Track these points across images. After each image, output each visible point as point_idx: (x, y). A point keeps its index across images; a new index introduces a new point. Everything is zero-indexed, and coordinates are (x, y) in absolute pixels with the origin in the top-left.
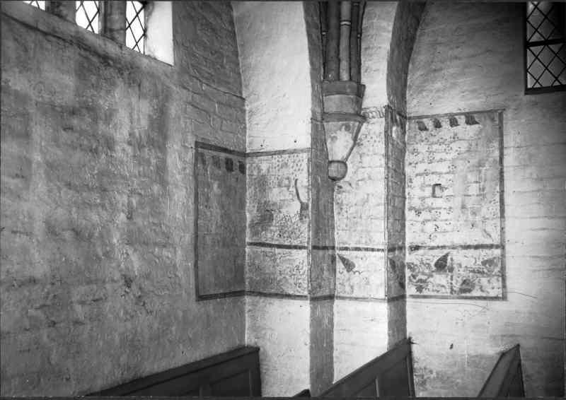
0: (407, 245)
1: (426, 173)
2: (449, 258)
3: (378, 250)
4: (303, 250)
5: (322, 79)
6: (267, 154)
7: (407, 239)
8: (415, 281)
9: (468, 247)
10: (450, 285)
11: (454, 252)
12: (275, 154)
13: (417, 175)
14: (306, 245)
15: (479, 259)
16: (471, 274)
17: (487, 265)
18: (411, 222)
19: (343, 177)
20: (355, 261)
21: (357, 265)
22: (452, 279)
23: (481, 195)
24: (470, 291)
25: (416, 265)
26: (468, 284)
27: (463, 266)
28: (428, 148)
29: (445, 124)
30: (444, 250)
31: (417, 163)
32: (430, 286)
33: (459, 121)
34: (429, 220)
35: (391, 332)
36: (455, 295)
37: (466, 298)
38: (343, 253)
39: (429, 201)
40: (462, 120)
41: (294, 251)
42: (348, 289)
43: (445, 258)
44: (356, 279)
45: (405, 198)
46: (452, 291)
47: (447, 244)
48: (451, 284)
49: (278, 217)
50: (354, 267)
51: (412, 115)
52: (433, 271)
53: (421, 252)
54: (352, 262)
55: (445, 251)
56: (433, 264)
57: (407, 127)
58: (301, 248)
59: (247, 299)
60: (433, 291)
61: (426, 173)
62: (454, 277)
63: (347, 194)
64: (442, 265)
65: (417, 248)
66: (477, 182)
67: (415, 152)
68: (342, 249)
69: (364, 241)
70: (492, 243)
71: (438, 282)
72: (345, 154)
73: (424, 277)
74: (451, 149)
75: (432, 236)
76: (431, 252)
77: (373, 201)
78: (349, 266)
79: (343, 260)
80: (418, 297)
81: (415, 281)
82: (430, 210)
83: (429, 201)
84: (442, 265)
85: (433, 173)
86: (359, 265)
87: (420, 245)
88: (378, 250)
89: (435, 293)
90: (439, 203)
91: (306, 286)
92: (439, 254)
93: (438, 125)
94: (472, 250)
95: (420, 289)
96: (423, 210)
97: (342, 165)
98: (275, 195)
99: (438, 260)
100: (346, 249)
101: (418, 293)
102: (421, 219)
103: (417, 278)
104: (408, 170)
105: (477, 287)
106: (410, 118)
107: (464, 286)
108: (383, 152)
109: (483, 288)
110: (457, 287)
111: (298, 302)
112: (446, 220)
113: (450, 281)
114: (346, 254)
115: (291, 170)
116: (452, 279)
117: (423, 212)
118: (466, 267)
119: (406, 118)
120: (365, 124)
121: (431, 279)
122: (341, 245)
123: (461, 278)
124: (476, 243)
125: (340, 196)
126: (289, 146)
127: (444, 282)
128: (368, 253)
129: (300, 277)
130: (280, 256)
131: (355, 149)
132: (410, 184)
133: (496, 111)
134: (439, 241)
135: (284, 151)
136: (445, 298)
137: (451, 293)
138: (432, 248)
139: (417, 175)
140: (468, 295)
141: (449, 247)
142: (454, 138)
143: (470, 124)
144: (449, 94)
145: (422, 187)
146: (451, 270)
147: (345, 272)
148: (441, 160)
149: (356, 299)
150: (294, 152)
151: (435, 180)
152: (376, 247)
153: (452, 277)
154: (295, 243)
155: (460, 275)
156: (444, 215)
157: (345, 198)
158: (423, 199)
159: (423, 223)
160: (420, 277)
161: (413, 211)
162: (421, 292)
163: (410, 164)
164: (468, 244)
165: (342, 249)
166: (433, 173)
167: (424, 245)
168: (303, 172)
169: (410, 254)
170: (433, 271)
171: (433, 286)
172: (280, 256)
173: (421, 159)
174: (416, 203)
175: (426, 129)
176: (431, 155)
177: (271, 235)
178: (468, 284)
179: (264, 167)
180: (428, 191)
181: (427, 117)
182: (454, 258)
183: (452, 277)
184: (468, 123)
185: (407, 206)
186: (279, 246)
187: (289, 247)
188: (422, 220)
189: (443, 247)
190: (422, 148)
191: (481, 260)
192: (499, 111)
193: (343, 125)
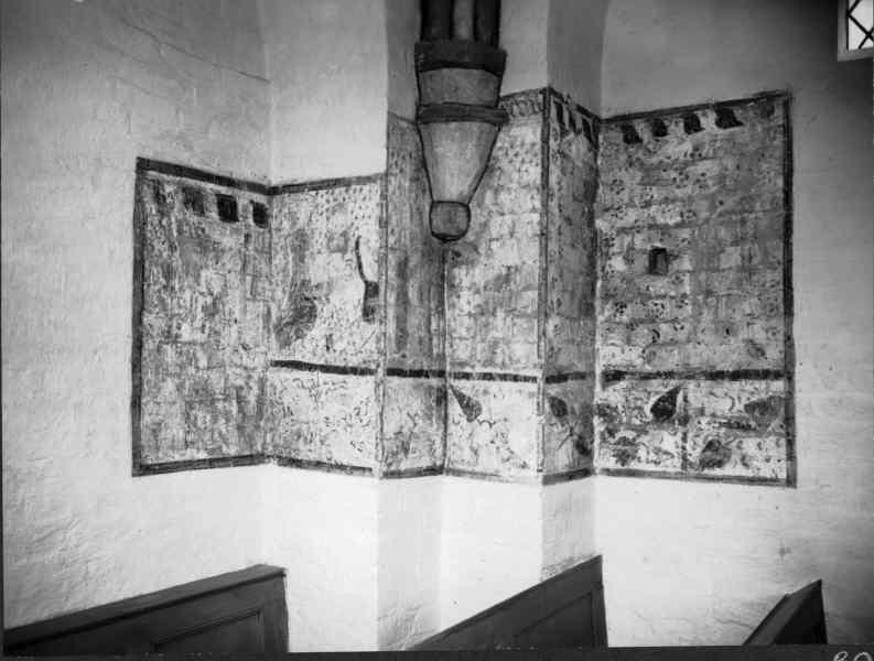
2: (680, 398)
11: (691, 385)
12: (321, 188)
15: (739, 398)
17: (757, 414)
20: (481, 399)
21: (484, 408)
22: (684, 439)
24: (720, 464)
27: (708, 412)
32: (642, 453)
36: (692, 472)
41: (351, 379)
48: (684, 448)
50: (480, 409)
53: (623, 384)
54: (478, 403)
55: (673, 383)
56: (647, 409)
58: (364, 372)
62: (690, 435)
73: (630, 435)
78: (471, 409)
79: (461, 398)
80: (617, 473)
87: (624, 370)
90: (659, 285)
92: (659, 388)
95: (623, 457)
99: (659, 400)
100: (467, 376)
105: (735, 457)
110: (695, 455)
114: (465, 386)
116: (684, 439)
121: (644, 439)
122: (458, 369)
140: (717, 472)
141: (681, 376)
147: (464, 421)
153: (685, 434)
180: (642, 262)
182: (691, 397)
183: (685, 434)
189: (670, 375)
191: (744, 401)
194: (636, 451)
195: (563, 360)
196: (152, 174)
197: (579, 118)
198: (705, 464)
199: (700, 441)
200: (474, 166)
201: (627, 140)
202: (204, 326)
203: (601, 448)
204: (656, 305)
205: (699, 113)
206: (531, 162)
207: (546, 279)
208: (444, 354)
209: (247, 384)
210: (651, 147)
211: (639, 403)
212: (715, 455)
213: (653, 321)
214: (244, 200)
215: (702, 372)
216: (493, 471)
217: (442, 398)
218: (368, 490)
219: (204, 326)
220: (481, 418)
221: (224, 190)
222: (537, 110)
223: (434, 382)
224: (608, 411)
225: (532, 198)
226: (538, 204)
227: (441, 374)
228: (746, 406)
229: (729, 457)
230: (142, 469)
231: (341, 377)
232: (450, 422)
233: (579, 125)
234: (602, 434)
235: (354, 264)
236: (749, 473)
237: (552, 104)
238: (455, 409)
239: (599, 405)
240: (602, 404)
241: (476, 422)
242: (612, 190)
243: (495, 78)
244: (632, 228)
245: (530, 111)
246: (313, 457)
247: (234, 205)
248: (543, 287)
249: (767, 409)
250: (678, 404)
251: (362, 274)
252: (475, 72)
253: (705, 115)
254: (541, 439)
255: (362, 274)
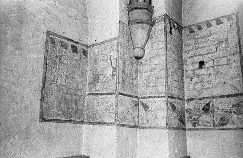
0: (186, 98)
1: (195, 56)
2: (211, 104)
3: (162, 97)
4: (113, 95)
5: (129, 3)
6: (99, 44)
7: (186, 94)
8: (191, 120)
9: (223, 96)
10: (212, 121)
11: (214, 100)
12: (101, 44)
13: (189, 58)
14: (115, 92)
15: (230, 103)
16: (226, 113)
17: (236, 107)
18: (188, 85)
19: (143, 57)
20: (149, 104)
21: (150, 107)
22: (213, 117)
23: (228, 64)
24: (225, 124)
25: (191, 110)
26: (224, 120)
27: (220, 108)
28: (195, 42)
29: (204, 27)
30: (207, 100)
31: (189, 51)
32: (200, 123)
33: (212, 23)
34: (198, 83)
35: (172, 149)
36: (216, 128)
37: (224, 129)
38: (142, 100)
39: (197, 72)
40: (213, 23)
41: (109, 96)
42: (145, 122)
43: (208, 104)
44: (150, 116)
45: (183, 70)
46: (214, 125)
47: (209, 96)
48: (213, 120)
49: (102, 78)
50: (149, 107)
51: (186, 26)
52: (202, 113)
53: (194, 101)
54: (147, 105)
55: (208, 100)
56: (201, 109)
57: (183, 32)
58: (112, 94)
59: (85, 127)
60: (202, 125)
61: (195, 56)
62: (215, 116)
63: (145, 66)
64: (207, 109)
65: (192, 99)
66: (225, 57)
67: (188, 45)
68: (142, 98)
69: (154, 92)
70: (238, 93)
71: (205, 119)
72: (143, 43)
73: (196, 117)
74: (209, 40)
75: (200, 91)
76: (200, 102)
77: (159, 67)
78: (146, 107)
79: (143, 104)
80: (193, 129)
81: (191, 120)
82: (198, 76)
83: (197, 72)
84: (207, 109)
85: (199, 55)
86: (152, 106)
87: (193, 98)
88: (162, 97)
89: (203, 127)
90: (203, 71)
91: (114, 116)
92: (204, 103)
93: (200, 28)
94: (225, 98)
95: (194, 125)
96: (194, 77)
97: (142, 49)
98: (101, 65)
99: (205, 106)
100: (145, 98)
101: (193, 127)
102: (193, 82)
103: (193, 118)
104: (184, 55)
105: (230, 122)
106: (184, 27)
107: (221, 121)
108: (164, 39)
109: (234, 122)
110: (217, 122)
111: (110, 127)
112: (208, 81)
113: (212, 119)
114: (145, 101)
115: (109, 51)
116: (213, 117)
117: (194, 79)
118: (222, 109)
119: (182, 28)
120: (154, 27)
121: (201, 118)
122: (142, 96)
123: (219, 116)
124: (227, 94)
125: (141, 68)
126: (109, 38)
127: (208, 120)
128: (157, 99)
129: (111, 111)
130: (101, 100)
131: (149, 41)
132: (186, 63)
133: (234, 14)
134: (205, 94)
135: (106, 41)
136: (210, 129)
137: (214, 126)
138: (201, 99)
139: (189, 58)
140: (225, 127)
141: (211, 98)
142: (210, 34)
143: (219, 24)
144: (239, 61)
145: (194, 63)
146: (213, 111)
147: (144, 111)
148: (203, 47)
149: (150, 127)
150: (111, 40)
151: (200, 59)
152: (160, 95)
153: (213, 116)
154: (110, 91)
155: (219, 114)
156: (206, 79)
157: (144, 69)
158: (193, 70)
159: (195, 84)
160: (194, 117)
161: (188, 78)
162: (195, 126)
163: (186, 52)
164: (223, 94)
165: (142, 98)
166: (199, 55)
167: (195, 97)
168: (115, 51)
169: (187, 103)
170: (202, 113)
171: (202, 122)
172: (101, 100)
173: (191, 49)
174: (190, 73)
175: (193, 32)
176: (197, 45)
177: (98, 88)
178: (224, 120)
179: (96, 51)
180: (197, 65)
181: (194, 25)
182: (214, 104)
183: (213, 116)
184: (217, 24)
185: (185, 76)
186: (101, 94)
187: (106, 94)
188: (194, 83)
189: (207, 98)
190: (192, 42)
191: (232, 104)
192: (236, 14)
193: (140, 26)
194: (199, 122)
195: (174, 92)
196: (51, 36)
197: (175, 25)
198: (222, 125)
199: (218, 117)
200: (146, 37)
201: (190, 32)
202: (65, 81)
203: (188, 122)
204: (202, 77)
205: (211, 22)
206: (161, 34)
207: (167, 67)
208: (138, 126)
209: (79, 99)
210: (197, 33)
211: (198, 107)
212: (223, 122)
213: (201, 82)
214: (79, 47)
215: (218, 96)
216: (153, 126)
217: (137, 105)
218: (113, 130)
219: (65, 81)
220: (149, 110)
221: (74, 44)
222: (163, 20)
223: (136, 100)
224: (189, 111)
225: (162, 44)
226: (164, 46)
227: (137, 97)
228: (232, 105)
229: (228, 122)
230: (43, 119)
231: (105, 96)
232: (140, 112)
233: (176, 27)
234: (188, 117)
235: (110, 63)
236: (235, 127)
237: (167, 19)
238: (141, 108)
239: (186, 109)
240: (187, 109)
241: (147, 111)
242: (187, 46)
243: (151, 13)
244: (193, 56)
245: (161, 21)
246: (97, 121)
247: (77, 49)
248: (166, 70)
249: (239, 106)
250: (210, 107)
251: (112, 66)
252: (145, 25)
253: (213, 22)
254: (167, 115)
255: (112, 66)
